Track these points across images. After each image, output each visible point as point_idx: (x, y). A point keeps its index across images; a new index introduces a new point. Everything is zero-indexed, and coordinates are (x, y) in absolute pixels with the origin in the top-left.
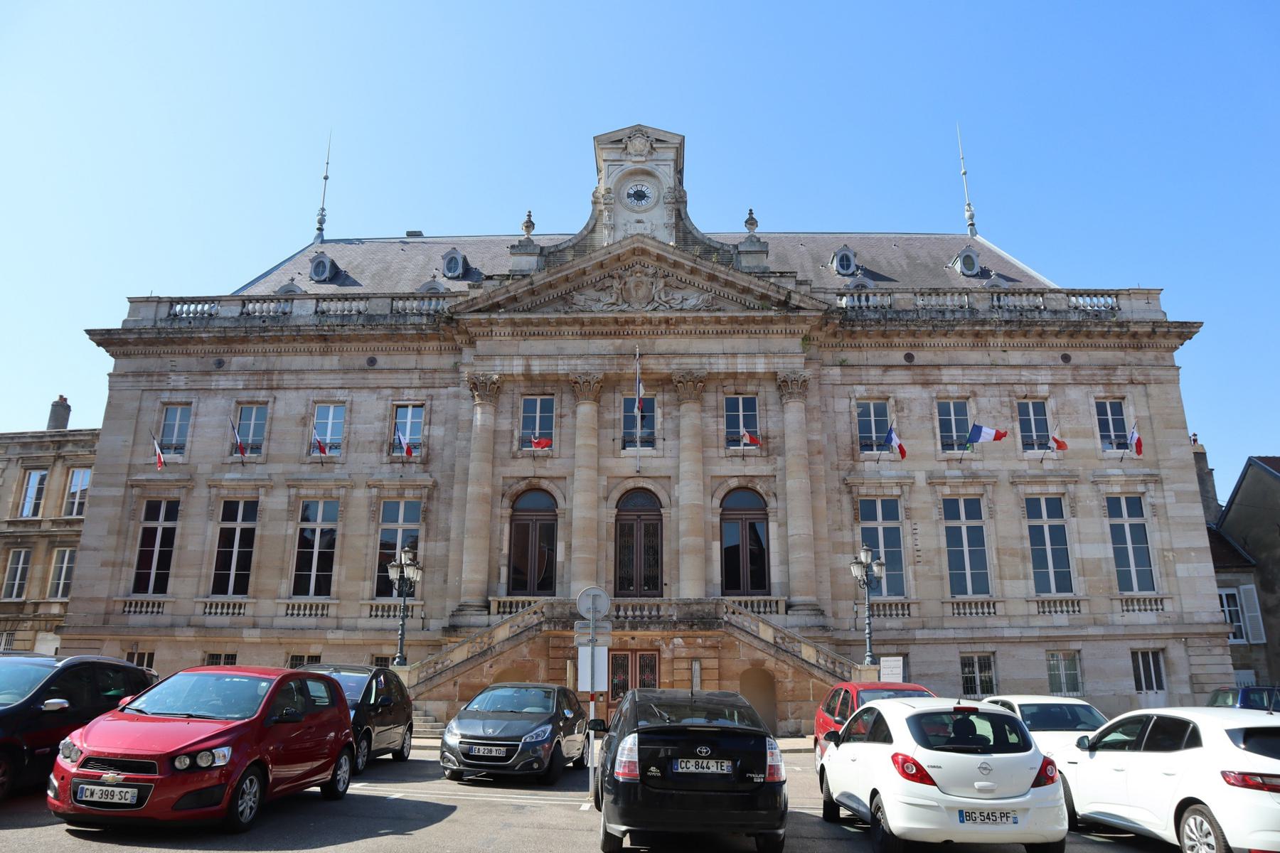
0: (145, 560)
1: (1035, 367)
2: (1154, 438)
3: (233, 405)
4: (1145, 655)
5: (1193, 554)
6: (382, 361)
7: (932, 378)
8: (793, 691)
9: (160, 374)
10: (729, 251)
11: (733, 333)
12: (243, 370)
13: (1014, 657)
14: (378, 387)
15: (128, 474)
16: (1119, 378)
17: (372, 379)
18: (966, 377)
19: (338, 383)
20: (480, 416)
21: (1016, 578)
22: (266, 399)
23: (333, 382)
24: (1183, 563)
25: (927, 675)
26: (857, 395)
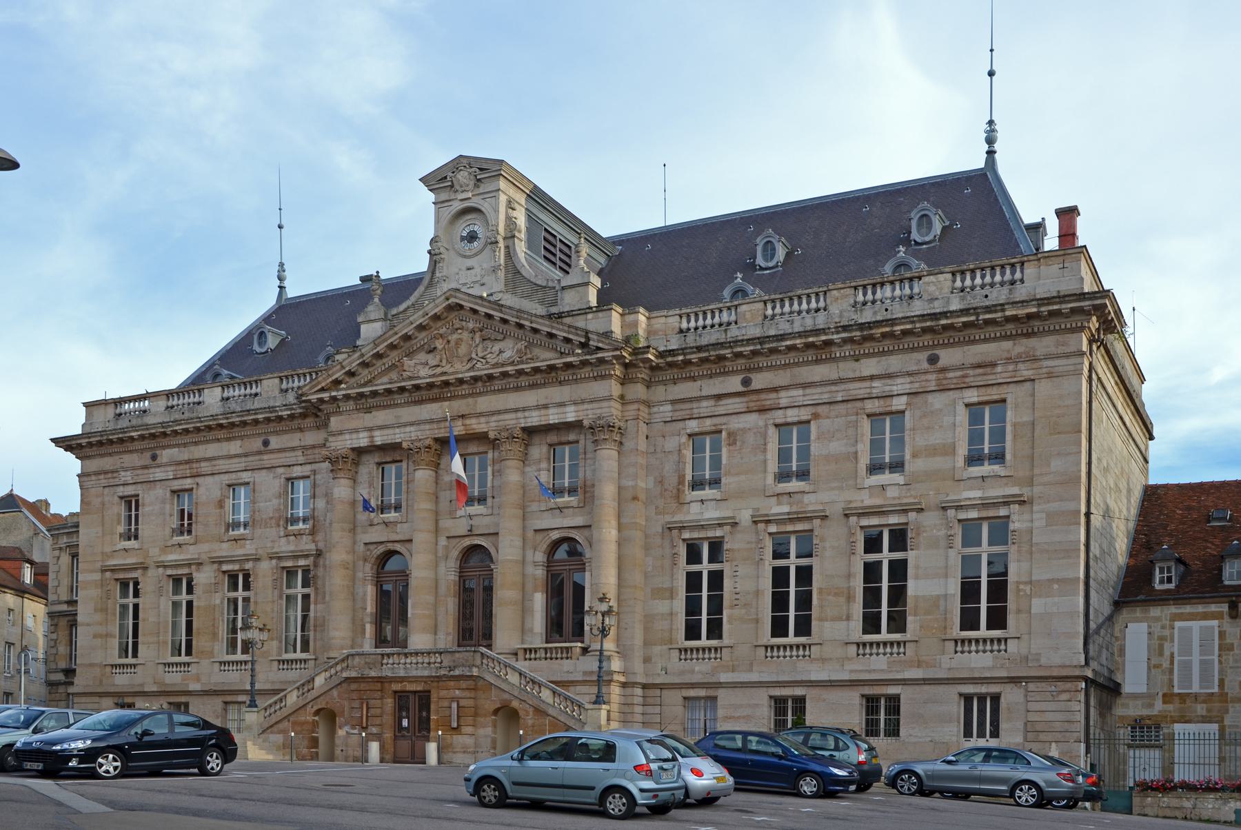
1: (889, 376)
2: (1033, 448)
3: (168, 494)
4: (982, 698)
5: (1056, 586)
6: (275, 442)
7: (768, 402)
8: (533, 726)
9: (113, 472)
10: (554, 288)
13: (824, 700)
14: (273, 467)
16: (998, 376)
17: (268, 459)
18: (808, 398)
20: (342, 490)
22: (191, 486)
23: (237, 465)
24: (1040, 596)
25: (734, 717)
26: (688, 431)
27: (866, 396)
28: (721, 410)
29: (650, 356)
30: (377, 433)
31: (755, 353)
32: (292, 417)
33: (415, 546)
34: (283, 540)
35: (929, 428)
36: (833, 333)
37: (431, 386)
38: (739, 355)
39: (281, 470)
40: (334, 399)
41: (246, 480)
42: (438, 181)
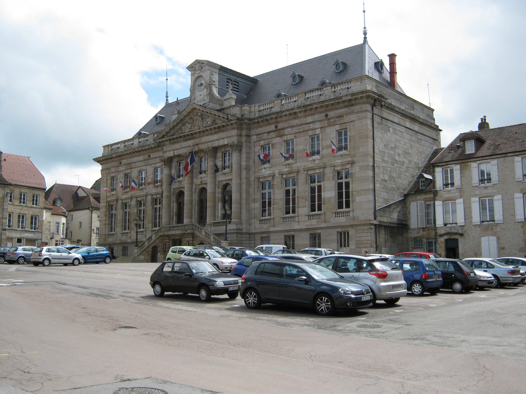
0: (340, 195)
5: (363, 192)
6: (152, 156)
11: (218, 132)
12: (126, 164)
14: (151, 164)
15: (106, 199)
17: (150, 162)
19: (143, 164)
21: (303, 207)
27: (308, 129)
28: (269, 137)
29: (246, 121)
30: (175, 151)
31: (276, 118)
32: (155, 147)
33: (233, 181)
34: (154, 189)
35: (326, 139)
36: (296, 110)
37: (188, 135)
38: (272, 119)
39: (153, 165)
40: (163, 141)
41: (144, 169)
42: (191, 68)
